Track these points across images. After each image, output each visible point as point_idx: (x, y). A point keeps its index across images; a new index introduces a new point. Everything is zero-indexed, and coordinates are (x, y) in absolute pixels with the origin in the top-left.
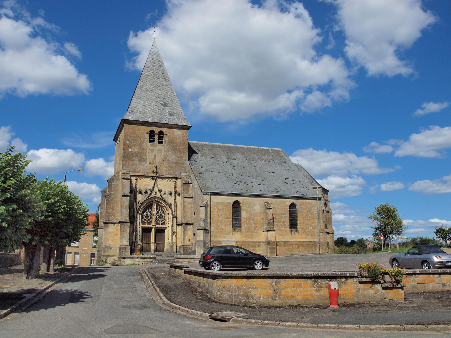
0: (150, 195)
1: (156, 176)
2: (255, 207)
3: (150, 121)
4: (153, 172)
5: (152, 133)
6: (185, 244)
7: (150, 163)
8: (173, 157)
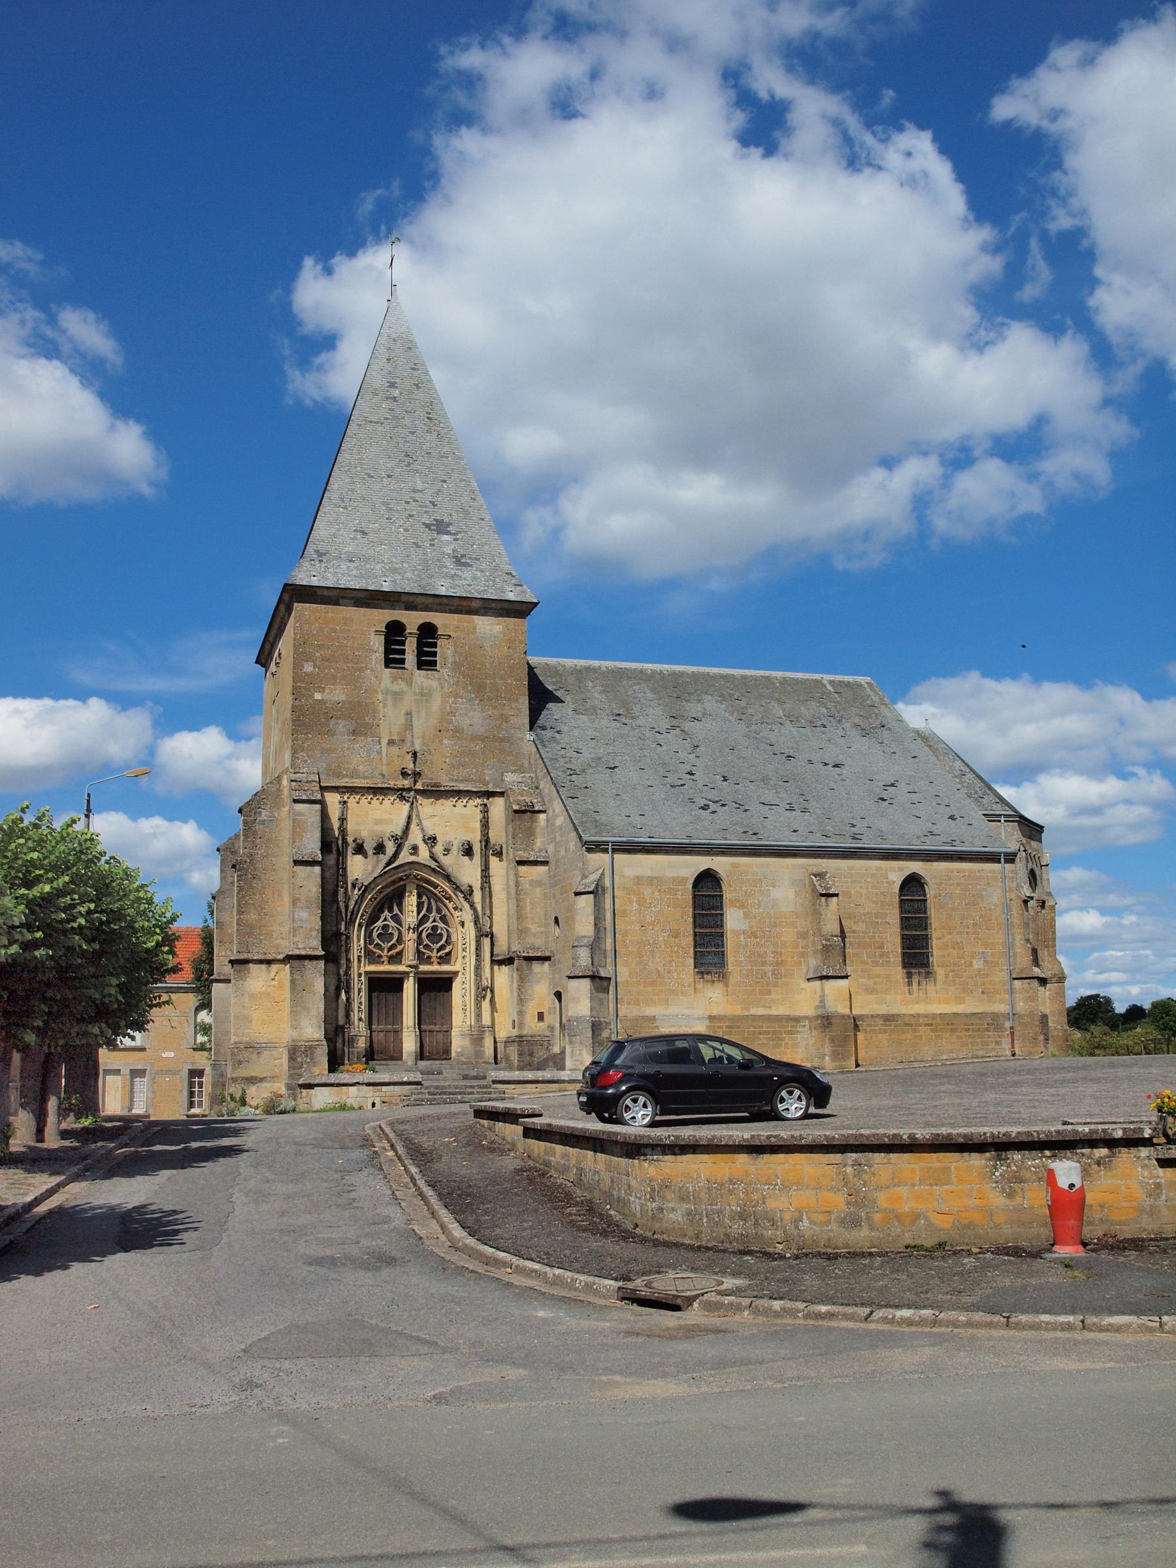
0: (395, 856)
1: (416, 787)
2: (776, 893)
3: (386, 587)
4: (404, 774)
5: (394, 631)
6: (525, 1032)
7: (391, 743)
8: (474, 718)
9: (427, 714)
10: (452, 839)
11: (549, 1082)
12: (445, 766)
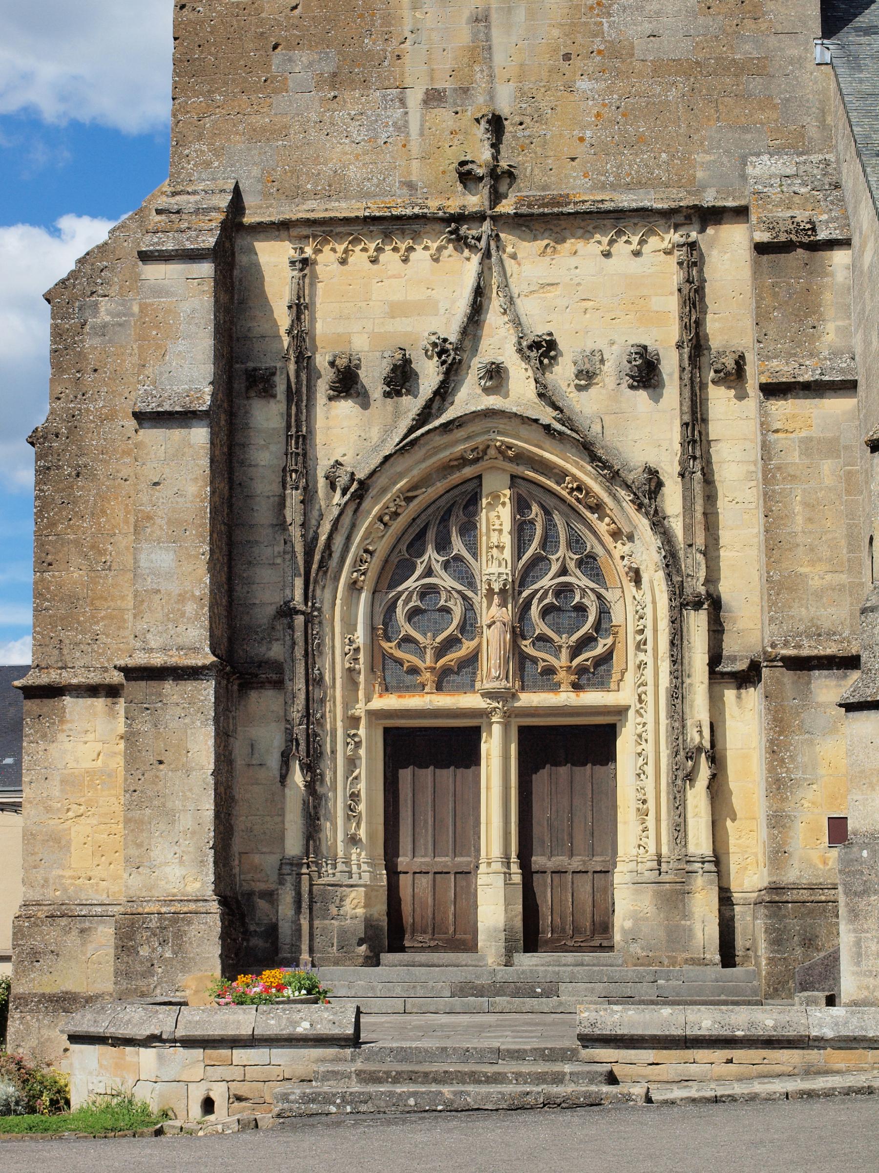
0: (444, 393)
1: (495, 207)
4: (466, 177)
6: (791, 876)
7: (434, 98)
9: (531, 15)
10: (601, 344)
11: (770, 1043)
12: (580, 150)
